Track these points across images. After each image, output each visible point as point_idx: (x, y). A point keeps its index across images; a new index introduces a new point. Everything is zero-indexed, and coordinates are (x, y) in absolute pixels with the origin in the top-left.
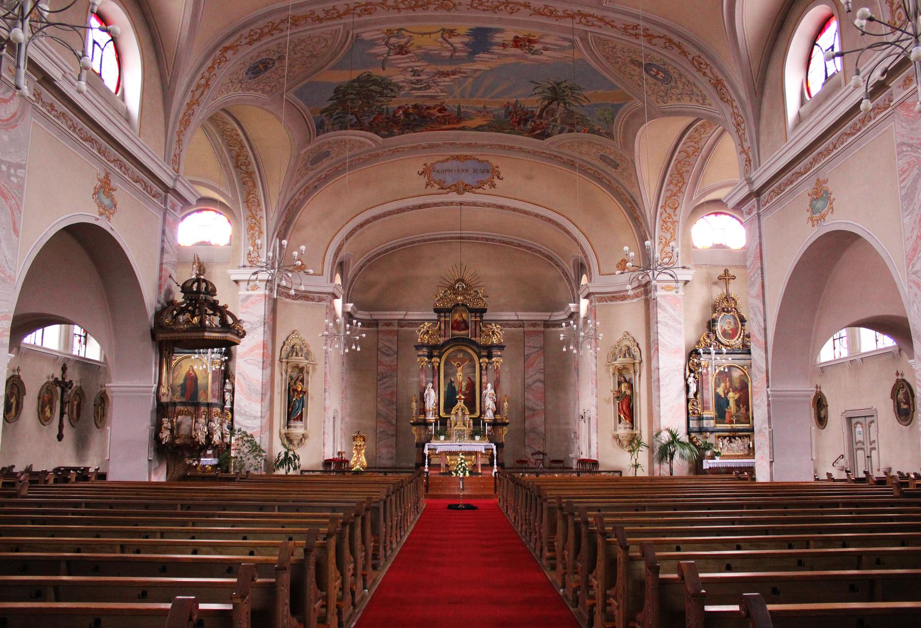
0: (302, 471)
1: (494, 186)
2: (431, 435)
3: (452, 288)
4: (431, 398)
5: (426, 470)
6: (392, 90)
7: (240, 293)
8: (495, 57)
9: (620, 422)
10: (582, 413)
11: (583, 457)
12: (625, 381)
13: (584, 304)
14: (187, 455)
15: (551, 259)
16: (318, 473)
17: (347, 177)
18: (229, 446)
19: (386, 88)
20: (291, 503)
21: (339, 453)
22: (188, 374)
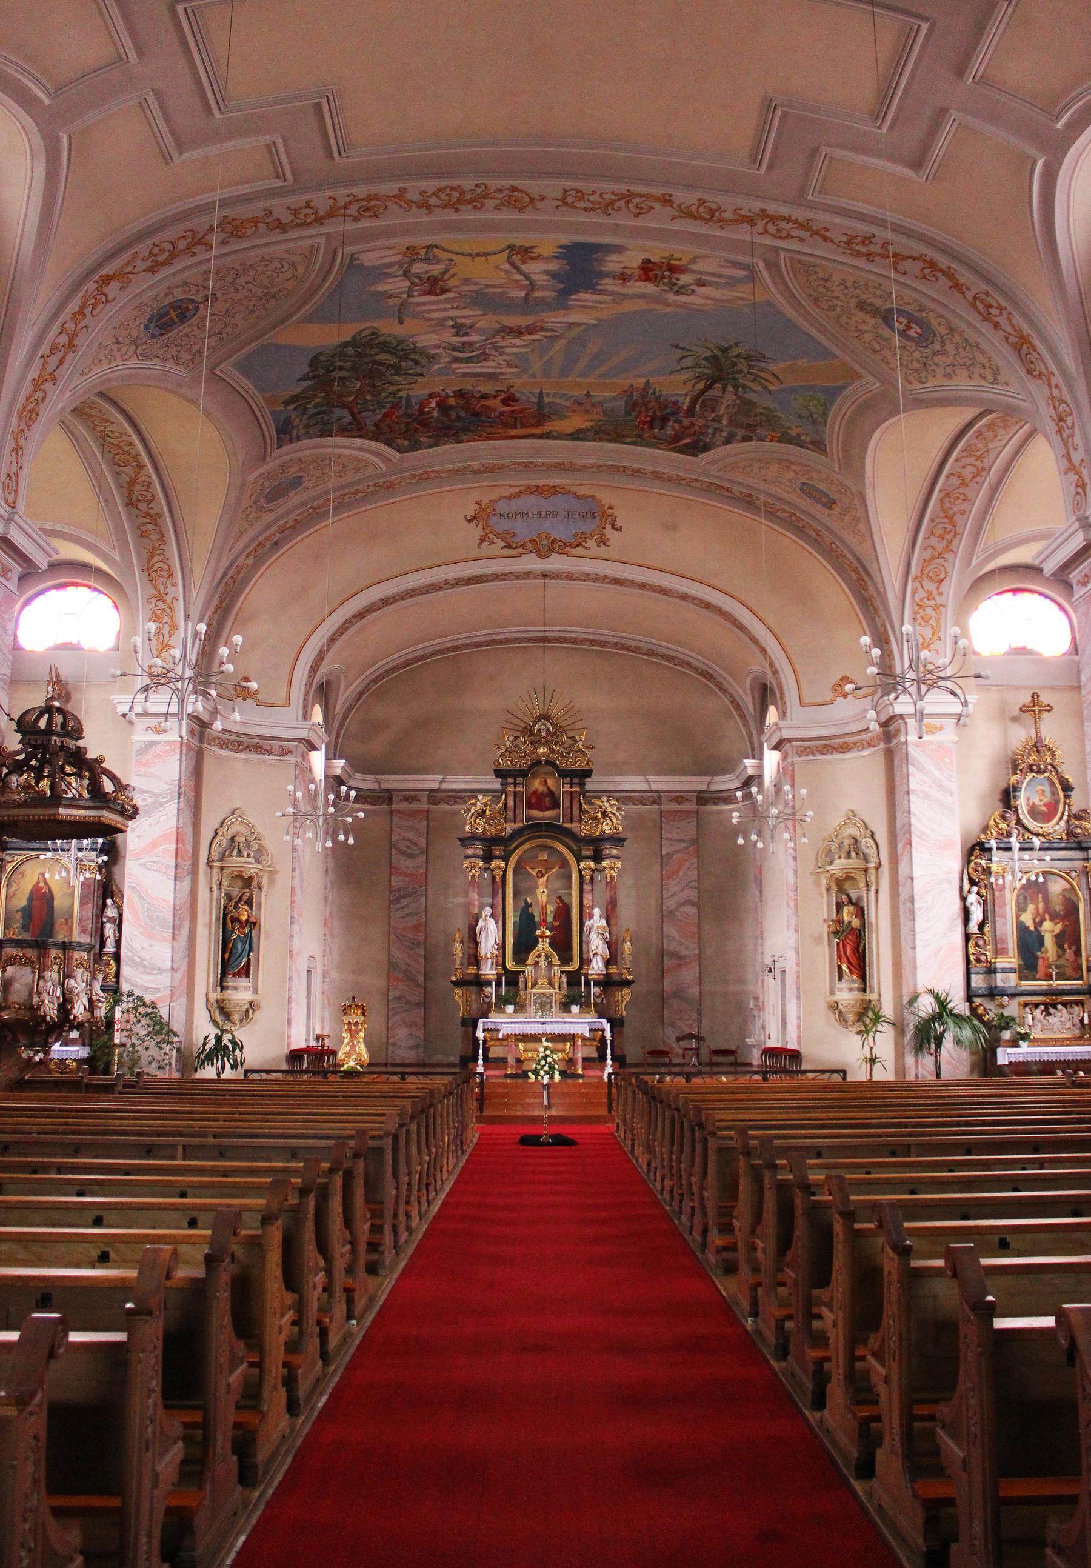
0: (246, 1072)
1: (604, 542)
2: (490, 1004)
4: (490, 935)
5: (480, 1069)
6: (417, 363)
7: (134, 738)
9: (840, 979)
10: (768, 961)
11: (772, 1044)
12: (850, 901)
13: (771, 759)
14: (23, 1040)
15: (710, 677)
16: (279, 1076)
17: (330, 527)
18: (110, 1022)
19: (405, 358)
20: (210, 1140)
21: (318, 1038)
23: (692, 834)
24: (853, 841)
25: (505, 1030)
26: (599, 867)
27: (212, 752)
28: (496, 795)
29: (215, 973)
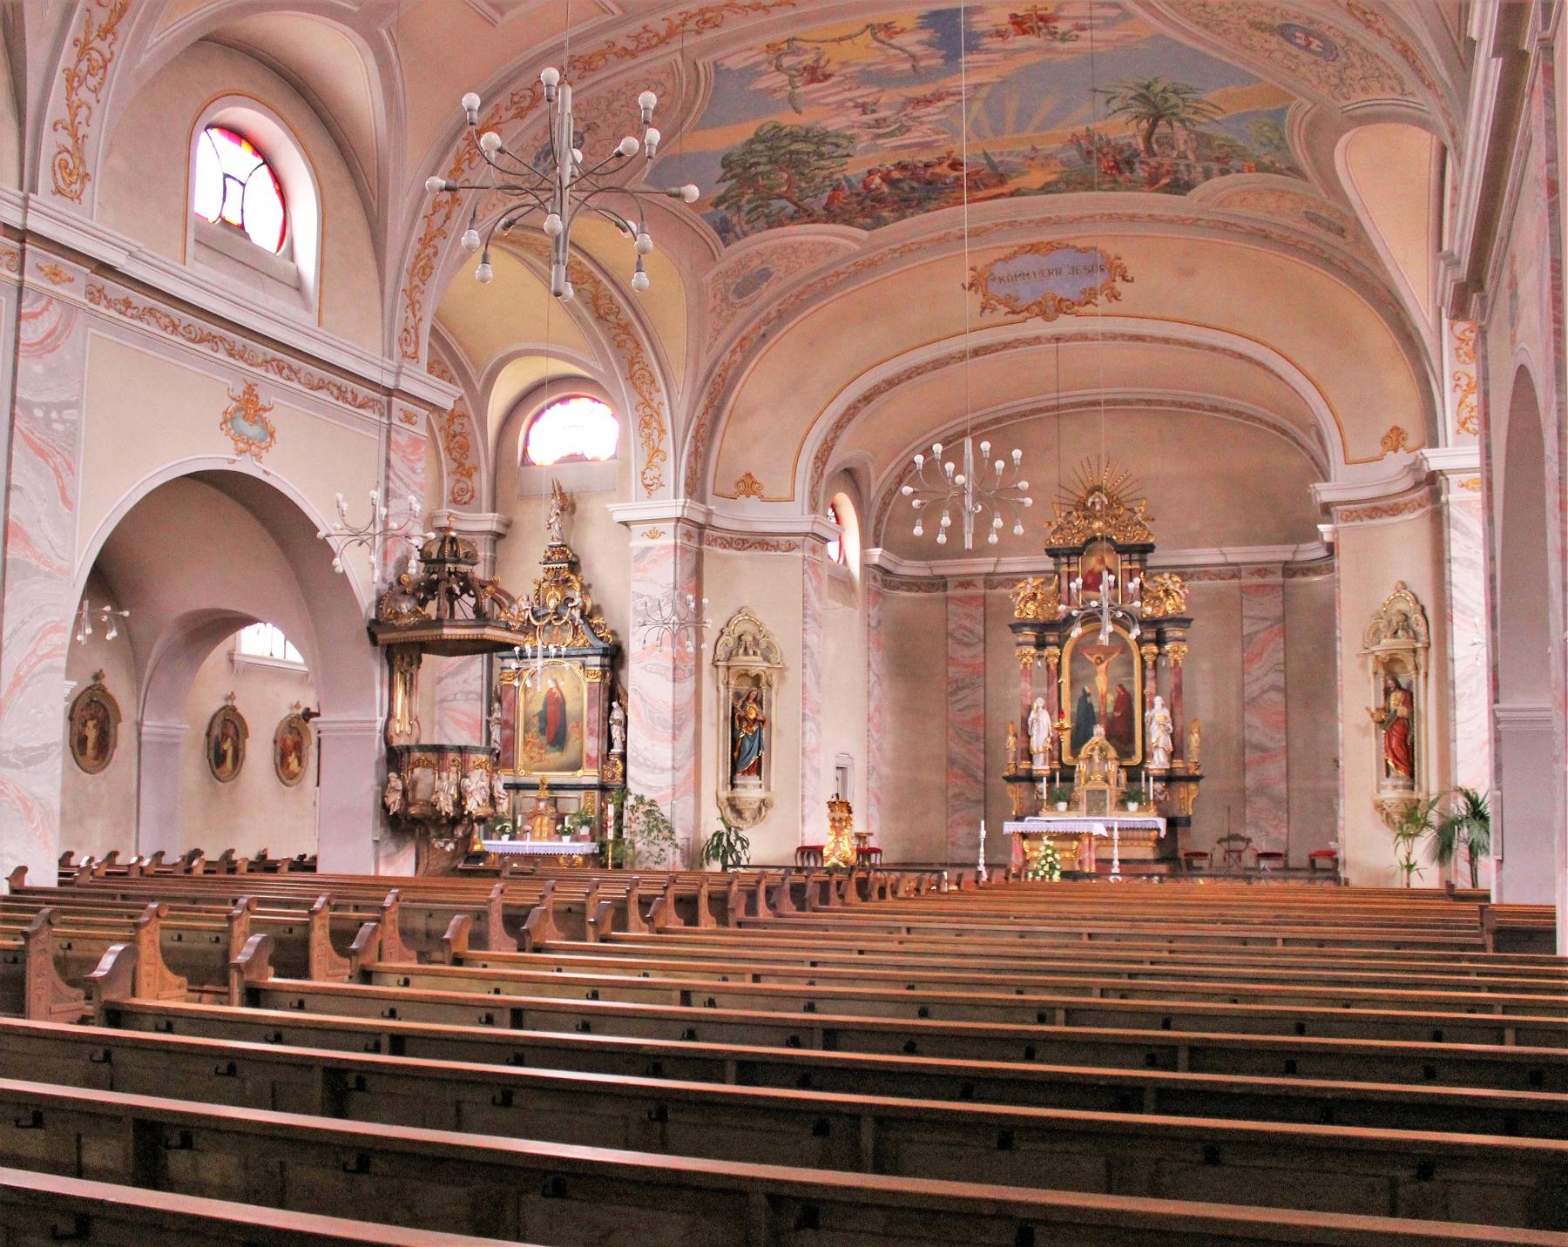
1: (1115, 296)
4: (1042, 728)
7: (632, 544)
8: (997, 56)
9: (1388, 775)
12: (1398, 686)
22: (550, 695)
23: (1277, 611)
24: (1402, 617)
27: (713, 552)
28: (1047, 576)
29: (725, 772)
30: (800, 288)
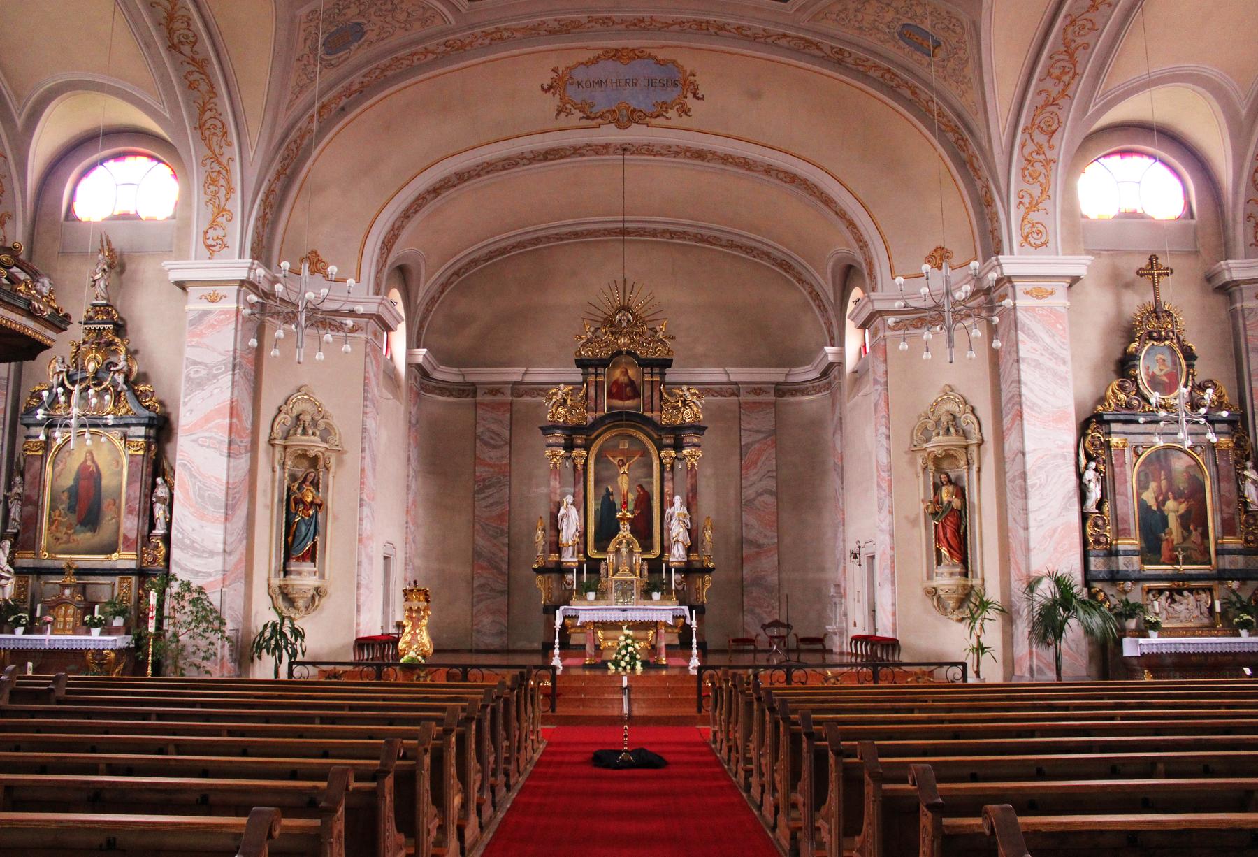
1: (685, 111)
2: (571, 591)
3: (608, 322)
7: (187, 308)
9: (939, 562)
12: (950, 481)
15: (786, 266)
22: (83, 469)
23: (769, 424)
25: (584, 617)
26: (680, 456)
30: (386, 61)
